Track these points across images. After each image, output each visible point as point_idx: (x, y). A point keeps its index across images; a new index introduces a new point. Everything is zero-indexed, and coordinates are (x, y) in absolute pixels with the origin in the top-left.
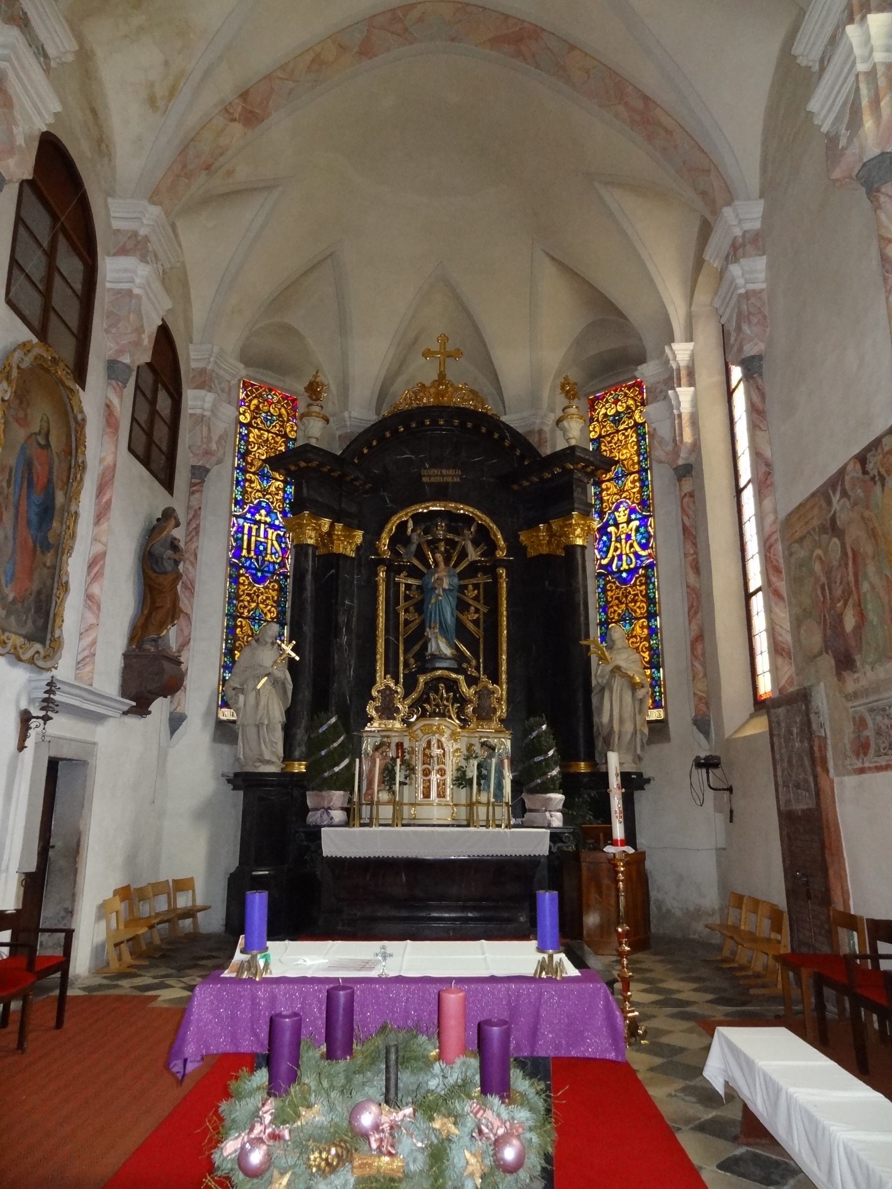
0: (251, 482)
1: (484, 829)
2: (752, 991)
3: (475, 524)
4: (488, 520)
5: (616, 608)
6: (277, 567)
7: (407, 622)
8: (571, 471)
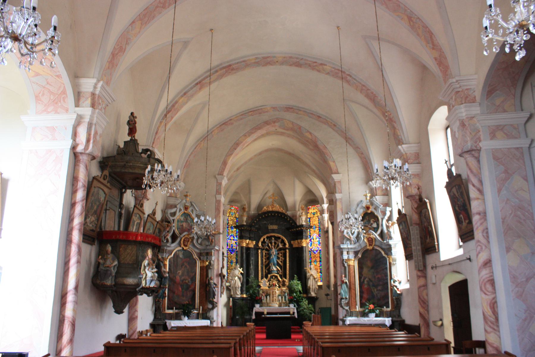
7: (265, 262)
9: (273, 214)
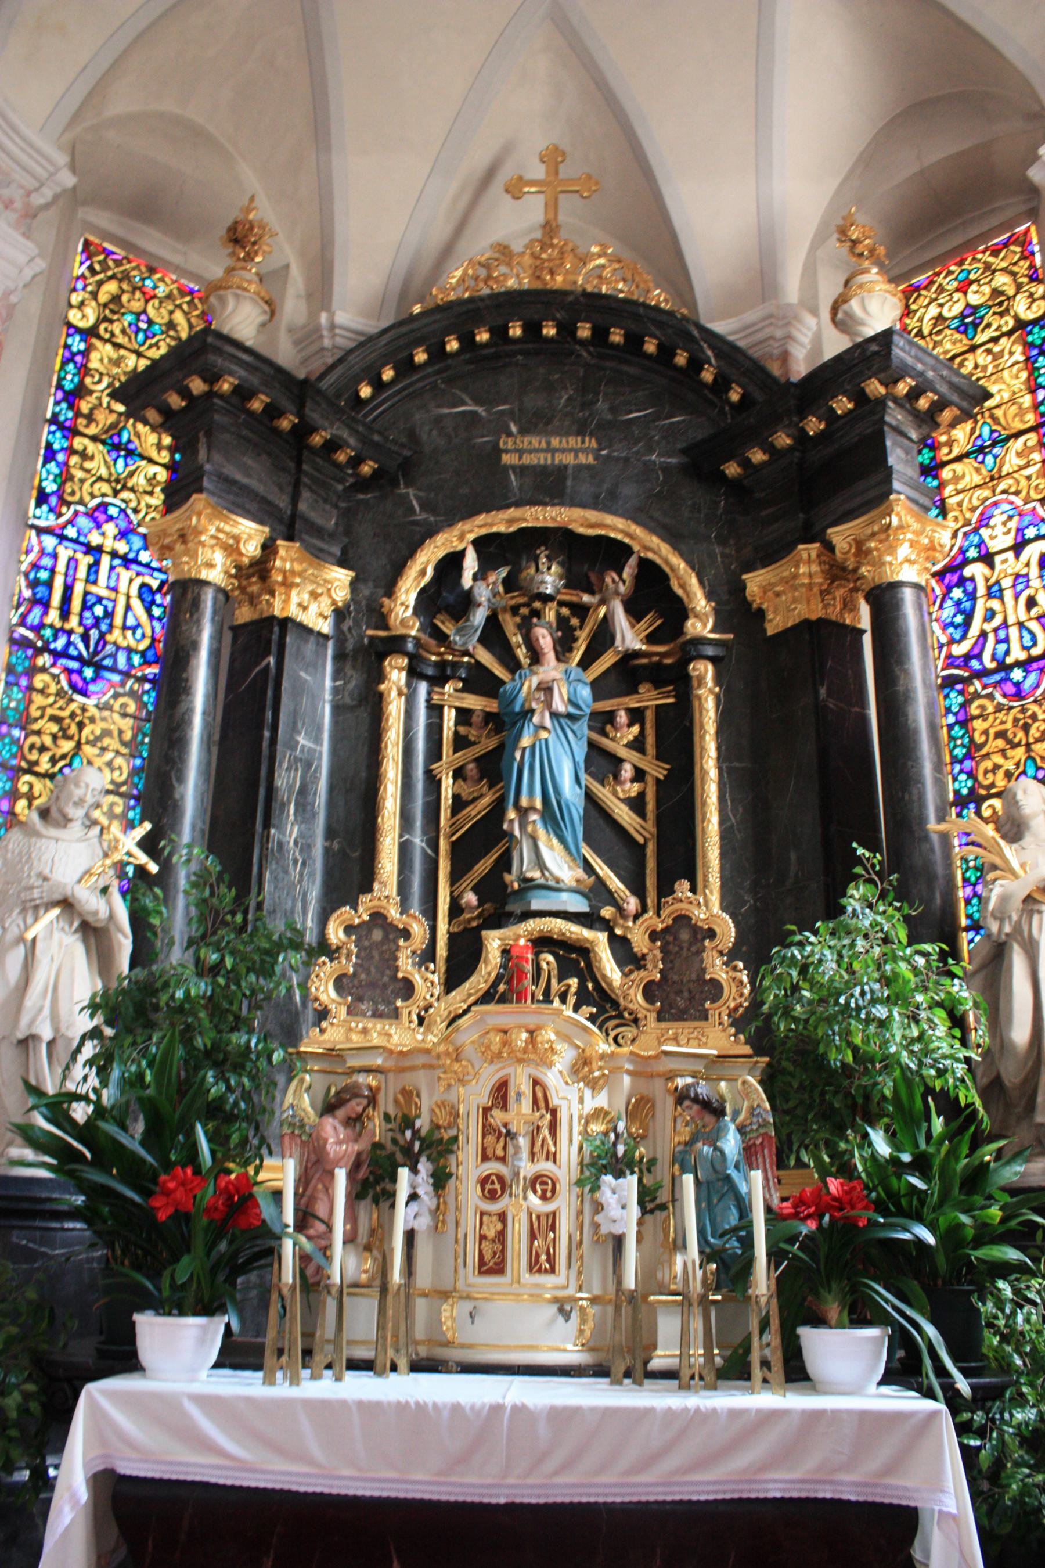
0: (84, 455)
1: (54, 383)
2: (630, 1282)
3: (633, 561)
4: (665, 549)
5: (998, 759)
6: (136, 660)
7: (459, 804)
8: (880, 403)
9: (550, 331)
